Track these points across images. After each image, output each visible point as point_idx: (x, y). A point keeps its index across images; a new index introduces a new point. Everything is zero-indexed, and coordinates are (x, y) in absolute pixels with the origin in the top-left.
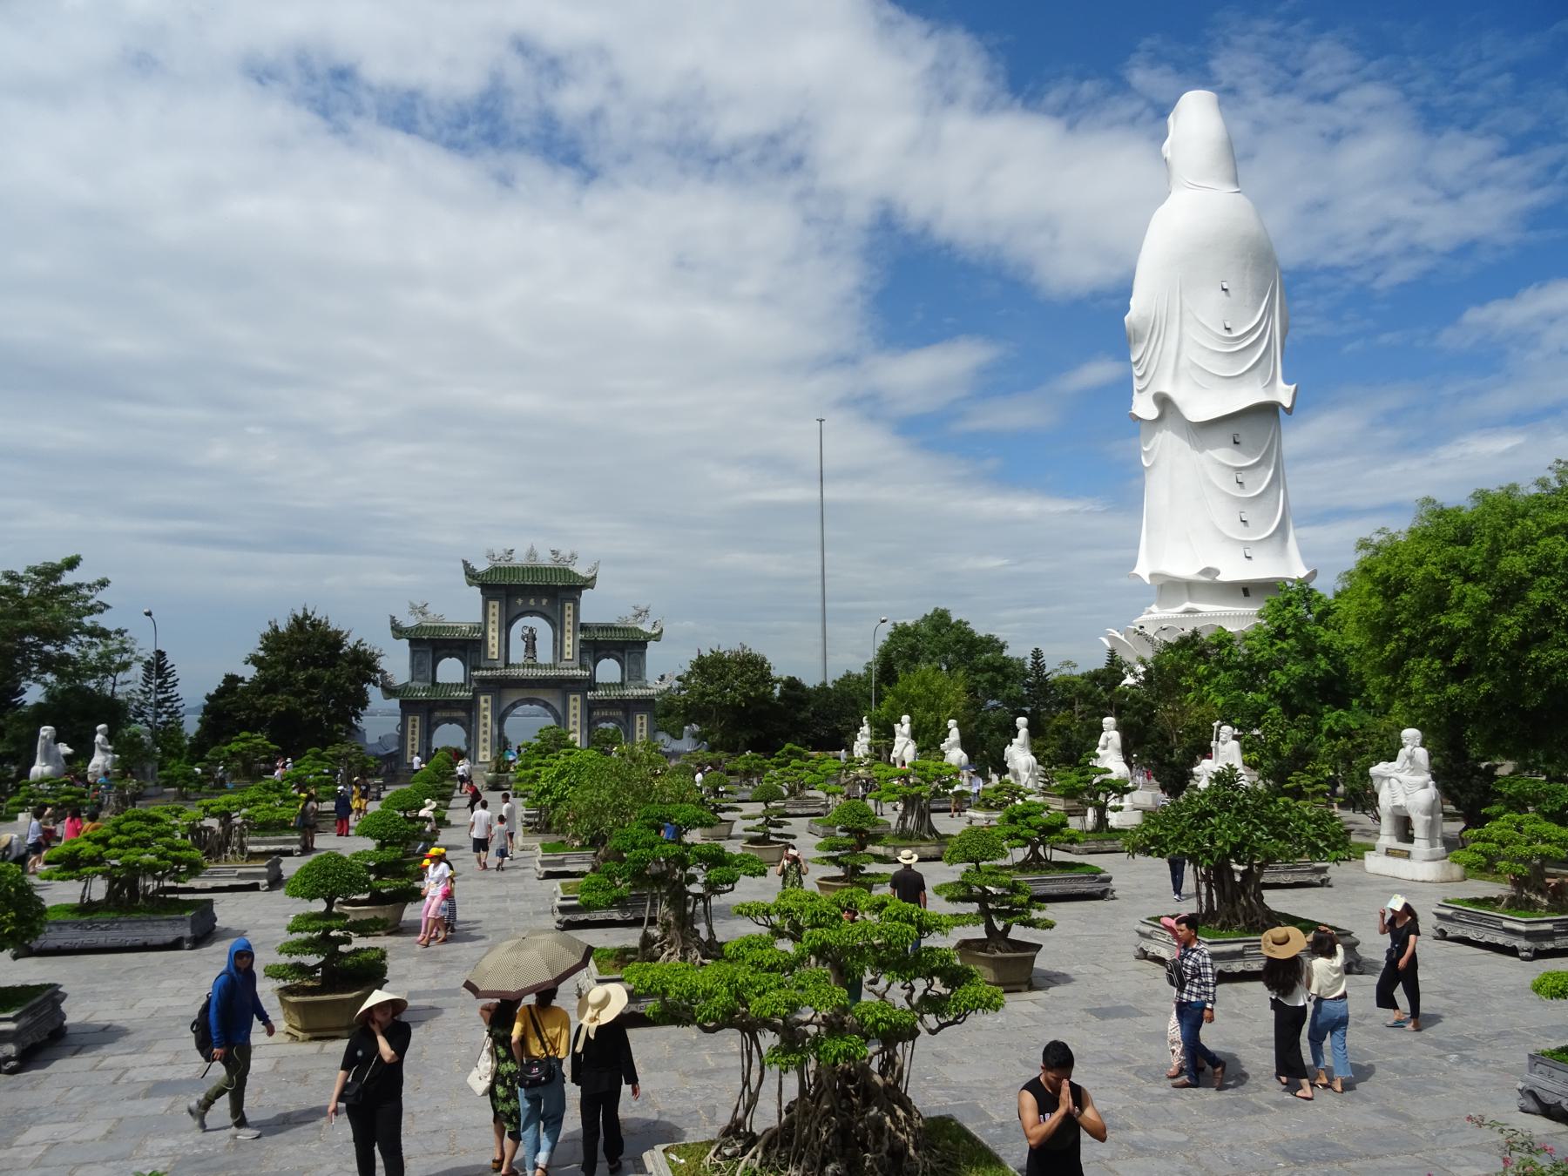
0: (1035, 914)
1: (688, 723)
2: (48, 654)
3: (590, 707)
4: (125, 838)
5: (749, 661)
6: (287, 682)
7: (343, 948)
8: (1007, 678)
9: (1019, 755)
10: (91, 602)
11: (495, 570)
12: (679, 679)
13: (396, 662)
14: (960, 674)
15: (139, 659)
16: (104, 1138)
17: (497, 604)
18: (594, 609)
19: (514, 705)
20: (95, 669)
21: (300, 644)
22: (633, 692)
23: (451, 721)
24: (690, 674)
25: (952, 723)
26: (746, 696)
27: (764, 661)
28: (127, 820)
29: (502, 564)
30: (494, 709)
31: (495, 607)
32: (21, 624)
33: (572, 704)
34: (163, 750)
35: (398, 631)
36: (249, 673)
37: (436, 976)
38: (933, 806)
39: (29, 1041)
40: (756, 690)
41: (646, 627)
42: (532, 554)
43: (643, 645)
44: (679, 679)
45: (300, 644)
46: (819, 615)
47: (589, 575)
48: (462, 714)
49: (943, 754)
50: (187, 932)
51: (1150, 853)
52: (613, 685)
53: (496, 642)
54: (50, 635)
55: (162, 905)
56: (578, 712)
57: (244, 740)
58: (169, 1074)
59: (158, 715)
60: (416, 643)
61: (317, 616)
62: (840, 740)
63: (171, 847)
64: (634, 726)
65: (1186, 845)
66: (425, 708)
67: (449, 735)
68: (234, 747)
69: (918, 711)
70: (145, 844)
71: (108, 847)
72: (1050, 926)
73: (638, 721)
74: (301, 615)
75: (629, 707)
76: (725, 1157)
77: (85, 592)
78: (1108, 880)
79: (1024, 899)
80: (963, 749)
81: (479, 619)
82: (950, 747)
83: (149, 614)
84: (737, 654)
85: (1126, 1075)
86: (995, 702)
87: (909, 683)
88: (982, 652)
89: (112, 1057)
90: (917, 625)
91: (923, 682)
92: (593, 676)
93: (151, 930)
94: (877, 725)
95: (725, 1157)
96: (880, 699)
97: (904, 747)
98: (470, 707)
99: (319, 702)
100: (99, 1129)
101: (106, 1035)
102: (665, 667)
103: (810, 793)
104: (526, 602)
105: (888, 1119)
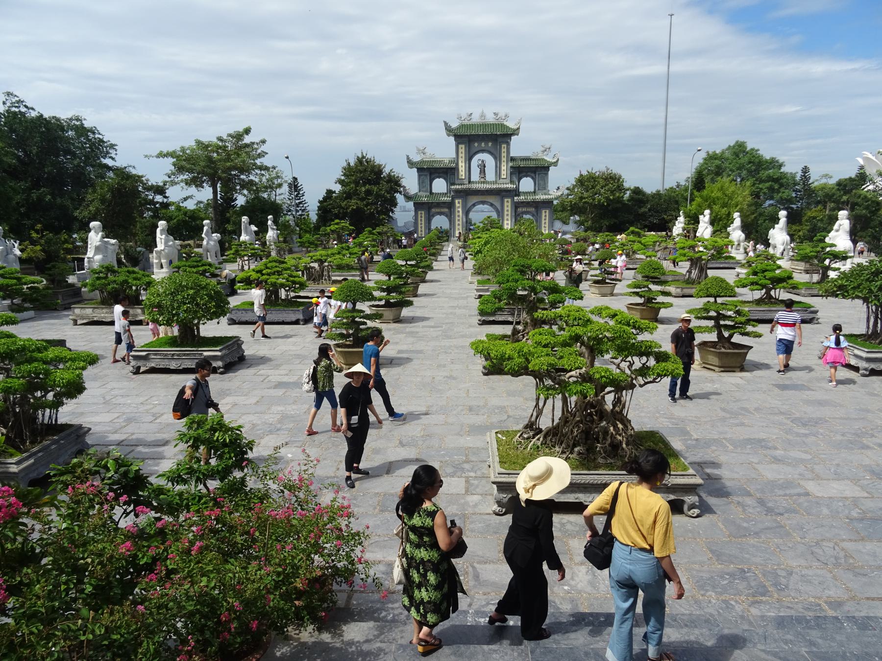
0: (749, 328)
1: (573, 214)
2: (243, 180)
3: (516, 206)
4: (269, 271)
5: (611, 178)
6: (356, 193)
7: (362, 327)
8: (781, 185)
9: (779, 235)
10: (259, 151)
11: (462, 126)
12: (568, 189)
13: (411, 181)
14: (748, 183)
15: (286, 182)
16: (255, 404)
17: (463, 146)
18: (518, 148)
19: (474, 205)
20: (266, 187)
21: (361, 172)
22: (541, 197)
23: (441, 214)
24: (574, 186)
25: (736, 215)
26: (607, 198)
27: (620, 177)
28: (270, 262)
29: (466, 122)
30: (464, 206)
31: (462, 148)
32: (228, 164)
33: (506, 204)
34: (301, 229)
35: (411, 164)
36: (337, 188)
37: (413, 343)
38: (709, 266)
39: (228, 361)
40: (614, 195)
41: (549, 159)
42: (483, 115)
43: (547, 169)
44: (568, 189)
45: (361, 172)
46: (662, 148)
47: (515, 127)
48: (446, 210)
49: (729, 234)
50: (301, 317)
51: (837, 296)
52: (529, 193)
53: (463, 169)
54: (242, 171)
55: (290, 303)
56: (509, 208)
57: (337, 224)
58: (285, 379)
59: (297, 211)
60: (420, 170)
61: (369, 156)
62: (665, 226)
63: (291, 276)
64: (541, 217)
65: (861, 292)
66: (427, 207)
67: (440, 222)
68: (333, 227)
69: (716, 208)
70: (279, 273)
71: (263, 275)
72: (760, 336)
73: (544, 214)
74: (360, 156)
75: (539, 206)
76: (524, 438)
77: (255, 146)
78: (816, 312)
79: (743, 319)
80: (743, 231)
81: (454, 156)
82: (734, 230)
83: (287, 158)
84: (604, 174)
85: (785, 421)
86: (771, 202)
87: (712, 190)
88: (765, 169)
89: (263, 370)
90: (723, 152)
91: (721, 189)
92: (518, 188)
93: (285, 315)
94: (689, 217)
95: (524, 438)
96: (692, 200)
97: (705, 229)
98: (450, 205)
99: (372, 204)
100: (254, 400)
101: (262, 360)
102: (560, 183)
103: (638, 256)
104: (480, 145)
105: (612, 428)
